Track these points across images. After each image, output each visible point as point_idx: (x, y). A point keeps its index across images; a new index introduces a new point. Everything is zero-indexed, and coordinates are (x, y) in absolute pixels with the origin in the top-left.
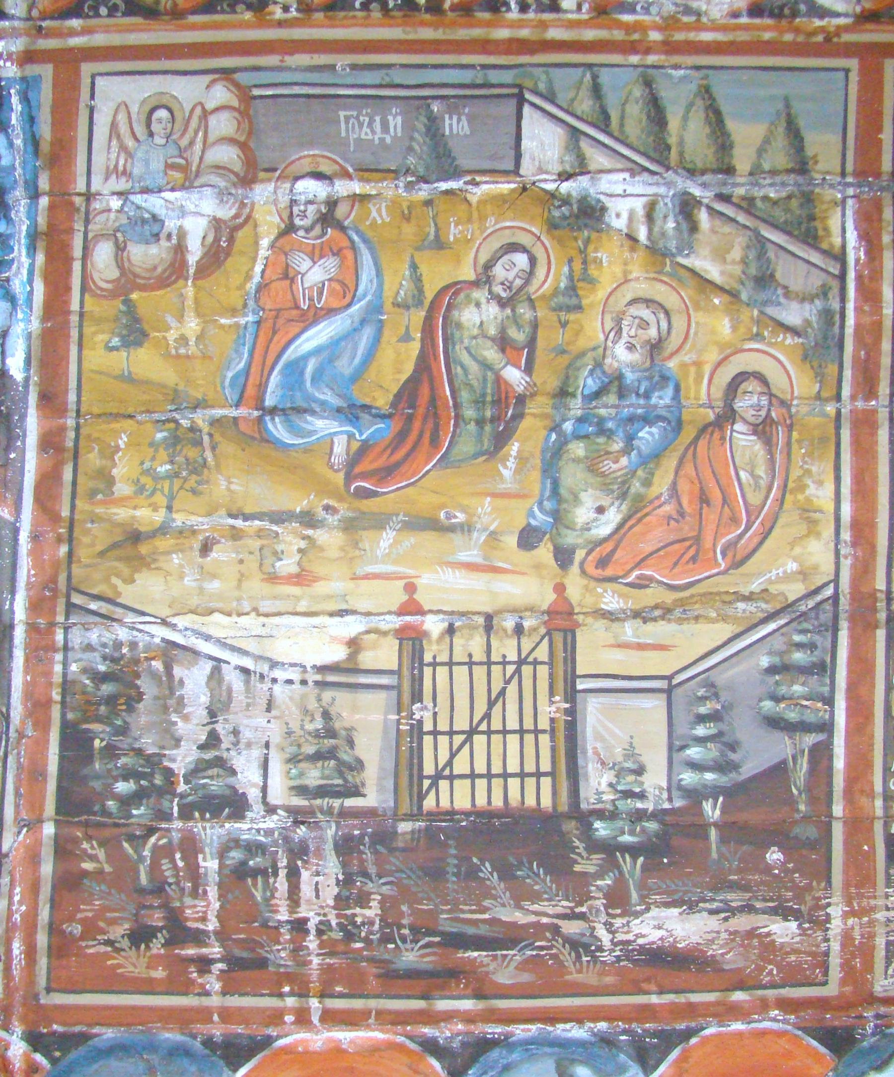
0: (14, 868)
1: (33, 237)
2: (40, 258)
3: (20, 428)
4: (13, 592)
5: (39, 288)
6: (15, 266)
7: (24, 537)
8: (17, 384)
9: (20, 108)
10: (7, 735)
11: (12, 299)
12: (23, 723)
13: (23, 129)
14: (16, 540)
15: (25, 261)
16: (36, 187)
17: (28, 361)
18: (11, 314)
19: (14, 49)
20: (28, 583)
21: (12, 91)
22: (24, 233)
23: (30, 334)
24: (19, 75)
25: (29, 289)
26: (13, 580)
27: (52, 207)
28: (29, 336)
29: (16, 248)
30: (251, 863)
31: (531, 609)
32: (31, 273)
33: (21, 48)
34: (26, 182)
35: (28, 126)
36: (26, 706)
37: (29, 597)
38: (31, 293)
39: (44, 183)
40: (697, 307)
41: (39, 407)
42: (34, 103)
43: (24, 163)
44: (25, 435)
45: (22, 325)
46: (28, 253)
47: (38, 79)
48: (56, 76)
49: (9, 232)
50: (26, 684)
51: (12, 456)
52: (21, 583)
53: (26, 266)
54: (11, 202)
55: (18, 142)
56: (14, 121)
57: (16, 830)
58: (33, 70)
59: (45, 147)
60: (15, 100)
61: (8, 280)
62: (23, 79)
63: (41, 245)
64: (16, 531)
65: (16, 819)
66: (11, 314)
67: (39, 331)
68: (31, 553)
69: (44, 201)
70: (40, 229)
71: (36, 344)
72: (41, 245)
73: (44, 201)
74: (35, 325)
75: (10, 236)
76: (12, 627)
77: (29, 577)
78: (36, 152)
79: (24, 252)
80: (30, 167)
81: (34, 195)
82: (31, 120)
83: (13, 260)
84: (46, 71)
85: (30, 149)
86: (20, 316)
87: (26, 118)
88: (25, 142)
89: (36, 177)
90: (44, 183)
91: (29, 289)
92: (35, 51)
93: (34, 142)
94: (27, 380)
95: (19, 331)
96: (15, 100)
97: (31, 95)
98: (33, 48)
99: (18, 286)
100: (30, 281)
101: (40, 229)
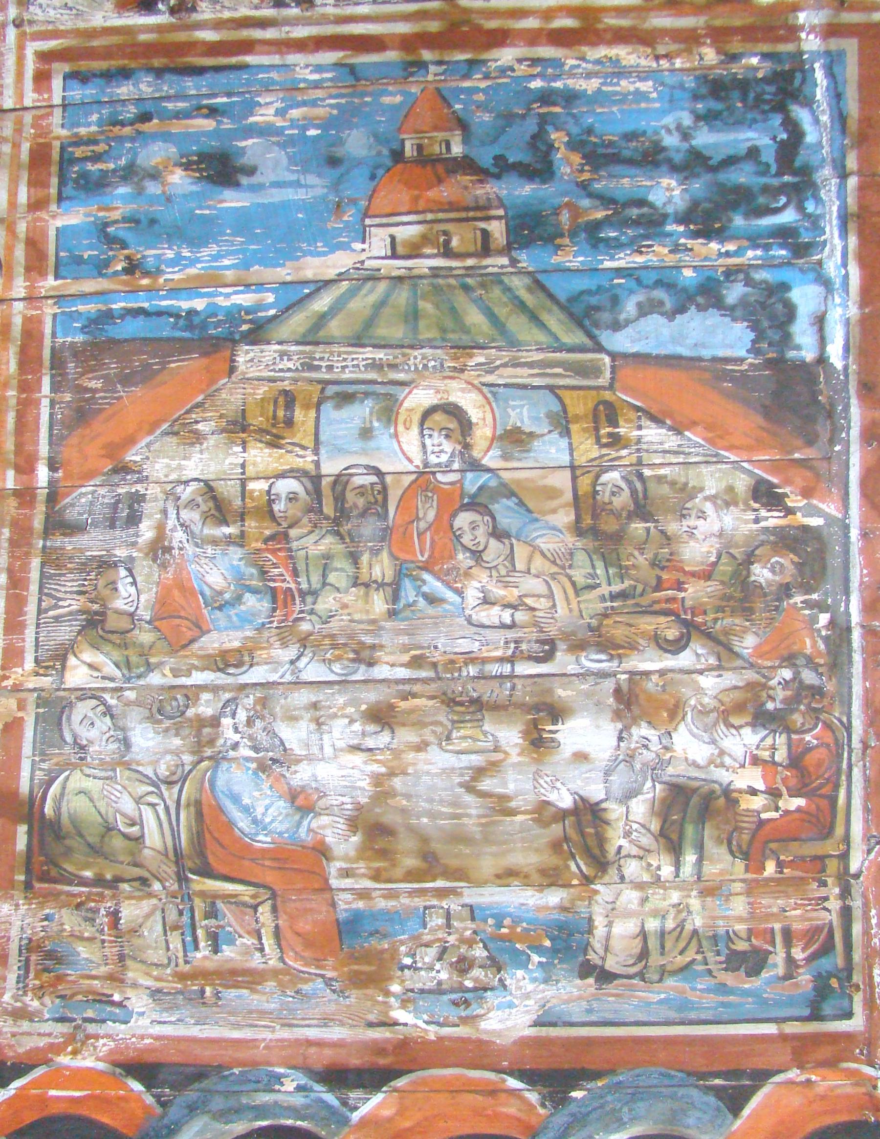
0: (866, 889)
1: (844, 220)
2: (853, 241)
3: (845, 418)
4: (847, 592)
5: (854, 272)
6: (827, 249)
7: (854, 533)
8: (838, 372)
9: (825, 83)
10: (849, 746)
11: (827, 284)
12: (866, 732)
13: (829, 105)
14: (847, 536)
15: (837, 242)
16: (844, 167)
17: (847, 348)
18: (826, 298)
19: (816, 21)
20: (861, 583)
21: (817, 66)
22: (835, 214)
23: (848, 319)
24: (822, 49)
25: (843, 272)
26: (847, 580)
27: (861, 188)
28: (847, 322)
29: (827, 229)
30: (519, 930)
31: (142, 827)
32: (845, 255)
33: (824, 21)
34: (833, 161)
35: (834, 102)
36: (867, 715)
37: (863, 598)
38: (846, 276)
39: (852, 162)
40: (39, 698)
41: (860, 397)
42: (839, 78)
43: (831, 140)
44: (849, 428)
45: (839, 311)
46: (840, 236)
47: (841, 54)
48: (861, 51)
49: (818, 212)
50: (866, 691)
51: (837, 448)
52: (855, 584)
53: (839, 248)
54: (819, 181)
55: (825, 118)
56: (819, 97)
57: (865, 848)
58: (834, 44)
59: (853, 125)
60: (819, 75)
61: (820, 263)
62: (828, 53)
63: (852, 226)
64: (847, 527)
65: (864, 835)
66: (826, 298)
67: (858, 317)
68: (862, 551)
69: (852, 182)
70: (850, 211)
71: (856, 331)
72: (852, 226)
73: (852, 182)
74: (853, 311)
75: (821, 216)
76: (849, 630)
77: (861, 576)
78: (844, 130)
79: (836, 233)
80: (837, 144)
81: (843, 176)
82: (837, 96)
83: (825, 243)
84: (851, 46)
85: (837, 126)
86: (838, 300)
87: (832, 94)
88: (832, 117)
89: (844, 157)
90: (852, 162)
91: (843, 272)
92: (838, 25)
93: (841, 118)
94: (846, 368)
95: (837, 317)
96: (819, 75)
97: (836, 69)
98: (835, 21)
99: (832, 268)
100: (845, 265)
101: (850, 211)
